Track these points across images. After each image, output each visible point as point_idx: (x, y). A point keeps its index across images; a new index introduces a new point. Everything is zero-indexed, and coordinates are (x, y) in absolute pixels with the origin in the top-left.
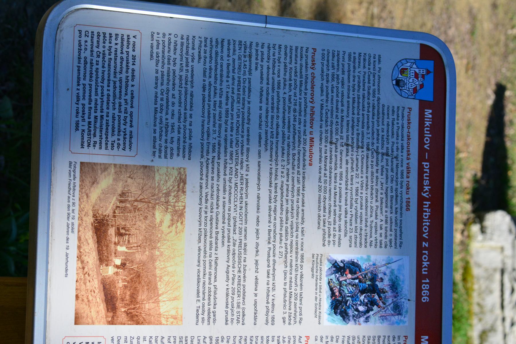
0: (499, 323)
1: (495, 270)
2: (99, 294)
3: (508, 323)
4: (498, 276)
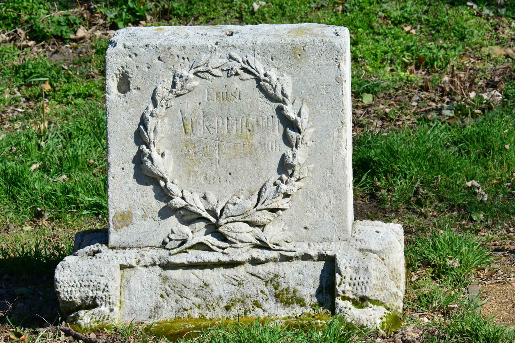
0: (260, 269)
1: (165, 279)
2: (294, 118)
3: (261, 254)
4: (176, 274)
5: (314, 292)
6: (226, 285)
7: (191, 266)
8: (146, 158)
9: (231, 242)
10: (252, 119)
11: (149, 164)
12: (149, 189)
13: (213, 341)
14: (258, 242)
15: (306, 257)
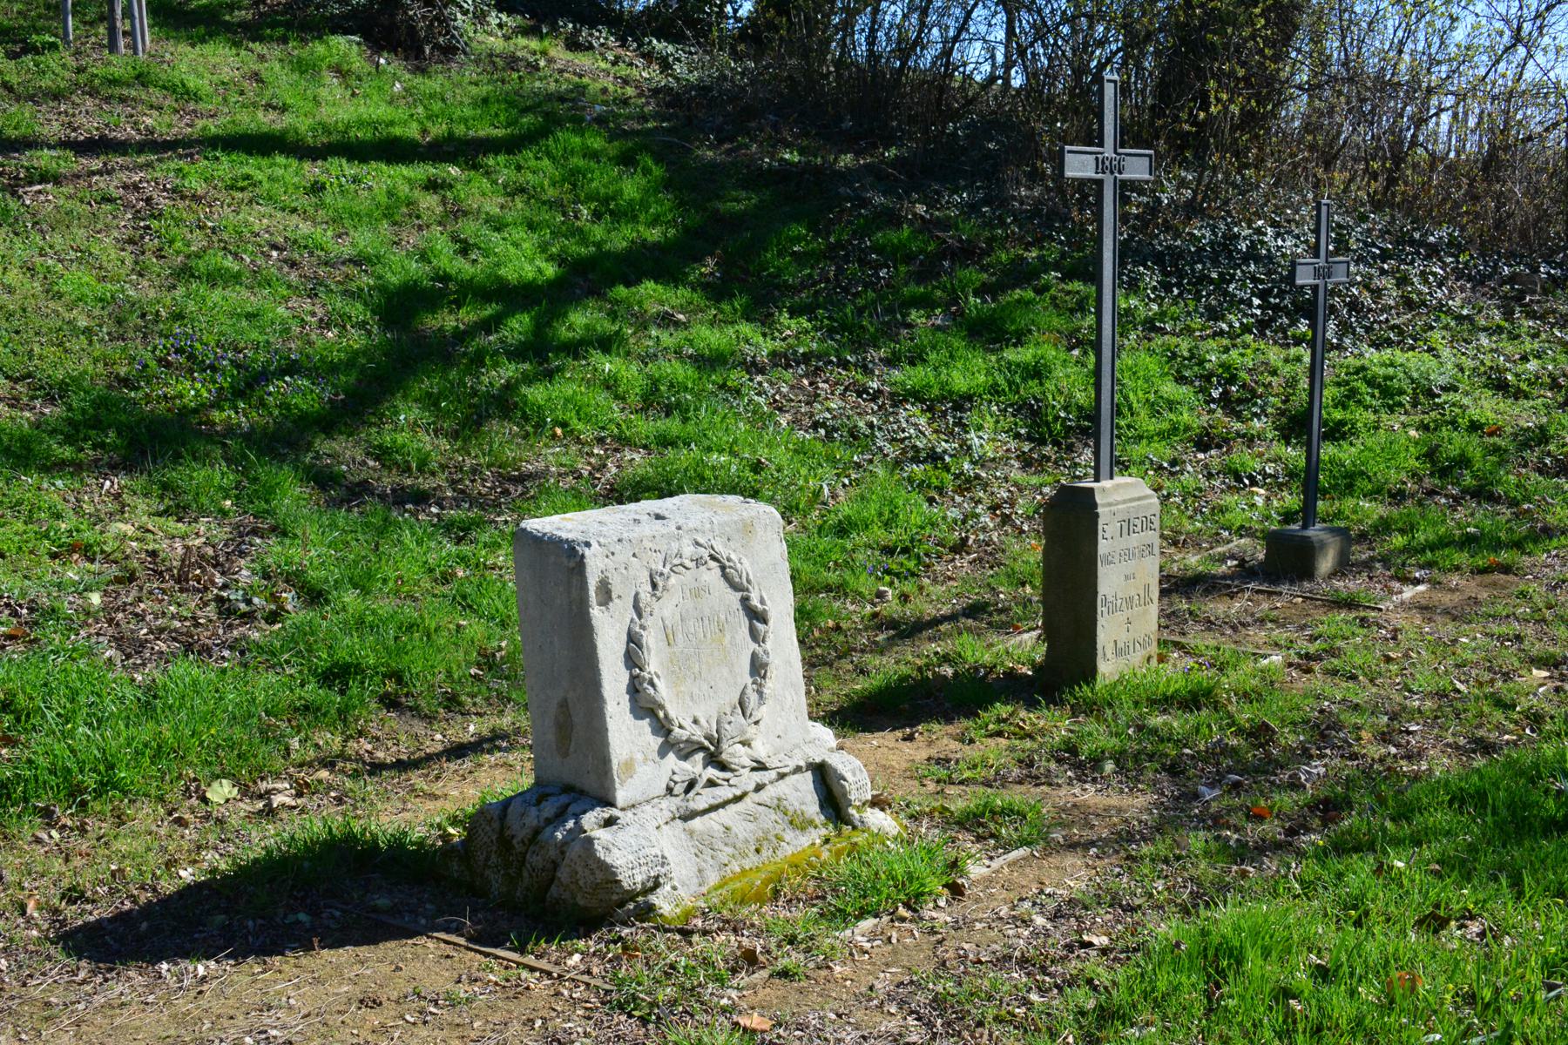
1: (691, 833)
4: (697, 823)
5: (818, 810)
6: (744, 823)
7: (713, 808)
8: (645, 685)
9: (733, 771)
10: (723, 617)
11: (651, 691)
12: (645, 724)
13: (8, 719)
14: (755, 764)
15: (798, 770)
